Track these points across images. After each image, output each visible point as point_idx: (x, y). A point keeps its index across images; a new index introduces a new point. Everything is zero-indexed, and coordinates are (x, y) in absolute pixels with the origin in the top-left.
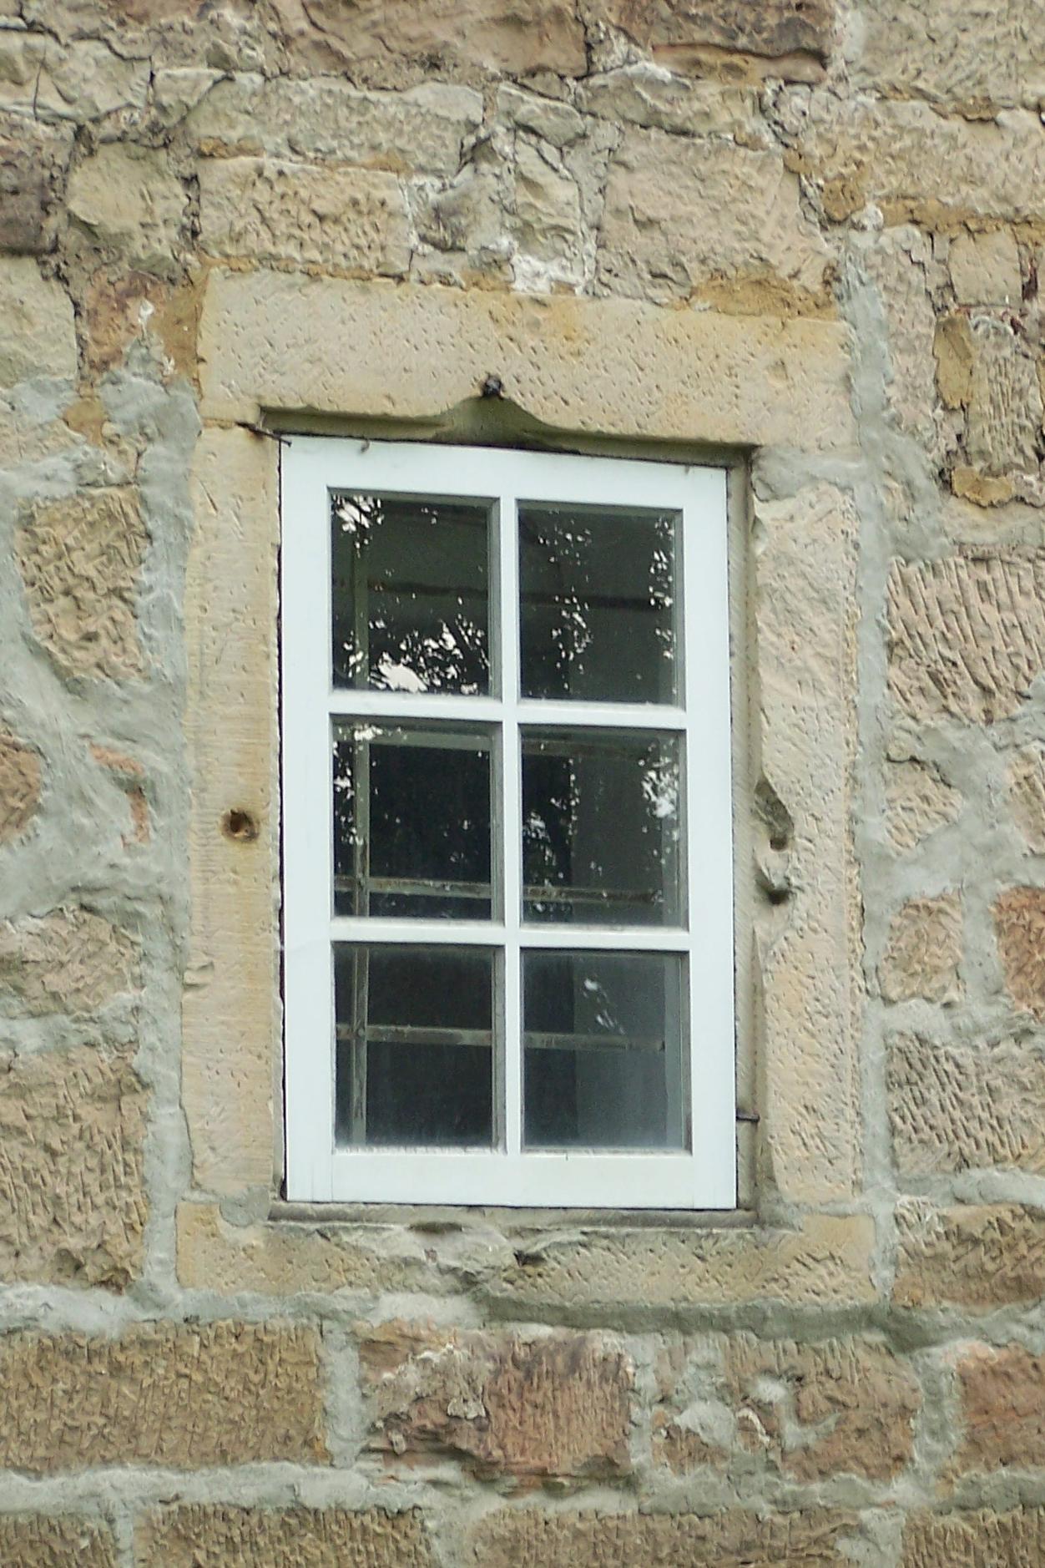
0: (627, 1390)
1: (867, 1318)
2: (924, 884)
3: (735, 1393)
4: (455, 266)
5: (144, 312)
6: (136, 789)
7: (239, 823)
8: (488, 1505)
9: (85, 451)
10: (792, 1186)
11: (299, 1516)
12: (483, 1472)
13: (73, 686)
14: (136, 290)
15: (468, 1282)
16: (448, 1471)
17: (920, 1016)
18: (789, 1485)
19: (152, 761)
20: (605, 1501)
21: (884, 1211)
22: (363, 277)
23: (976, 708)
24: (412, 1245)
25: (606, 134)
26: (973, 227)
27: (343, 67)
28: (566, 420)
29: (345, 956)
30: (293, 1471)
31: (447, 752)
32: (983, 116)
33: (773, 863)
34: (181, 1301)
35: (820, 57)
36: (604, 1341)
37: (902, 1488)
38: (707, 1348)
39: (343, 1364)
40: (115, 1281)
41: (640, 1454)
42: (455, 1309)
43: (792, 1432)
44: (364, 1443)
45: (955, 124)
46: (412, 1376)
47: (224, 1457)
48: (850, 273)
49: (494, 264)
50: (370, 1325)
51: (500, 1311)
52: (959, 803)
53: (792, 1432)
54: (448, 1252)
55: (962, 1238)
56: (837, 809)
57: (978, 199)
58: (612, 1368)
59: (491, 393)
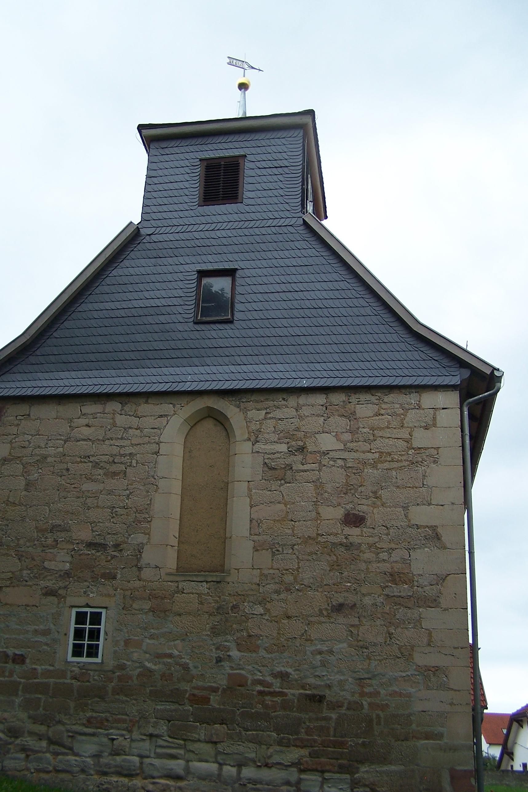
0: (90, 676)
1: (110, 671)
2: (118, 639)
3: (99, 676)
4: (85, 595)
5: (63, 599)
6: (58, 632)
7: (66, 634)
8: (79, 683)
9: (57, 609)
10: (104, 661)
11: (64, 683)
12: (79, 681)
13: (54, 625)
14: (62, 598)
15: (79, 667)
16: (76, 681)
17: (117, 648)
18: (103, 683)
19: (60, 630)
20: (88, 683)
21: (112, 663)
22: (78, 596)
23: (124, 625)
24: (76, 664)
25: (98, 585)
26: (127, 590)
27: (79, 582)
28: (92, 605)
29: (100, 625)
30: (64, 680)
31: (101, 619)
32: (129, 582)
33: (106, 637)
34: (57, 667)
35: (116, 579)
36: (89, 672)
37: (113, 684)
38: (97, 673)
39: (69, 672)
40: (53, 666)
41: (91, 680)
42: (78, 669)
43: (103, 679)
44: (303, 423)
45: (127, 583)
46: (74, 674)
47: (59, 679)
48: (116, 594)
49: (89, 595)
50: (71, 670)
51: (81, 669)
52: (122, 633)
53: (103, 679)
54: (79, 665)
55: (119, 665)
56: (111, 634)
57: (128, 588)
58: (89, 674)
59: (87, 604)
